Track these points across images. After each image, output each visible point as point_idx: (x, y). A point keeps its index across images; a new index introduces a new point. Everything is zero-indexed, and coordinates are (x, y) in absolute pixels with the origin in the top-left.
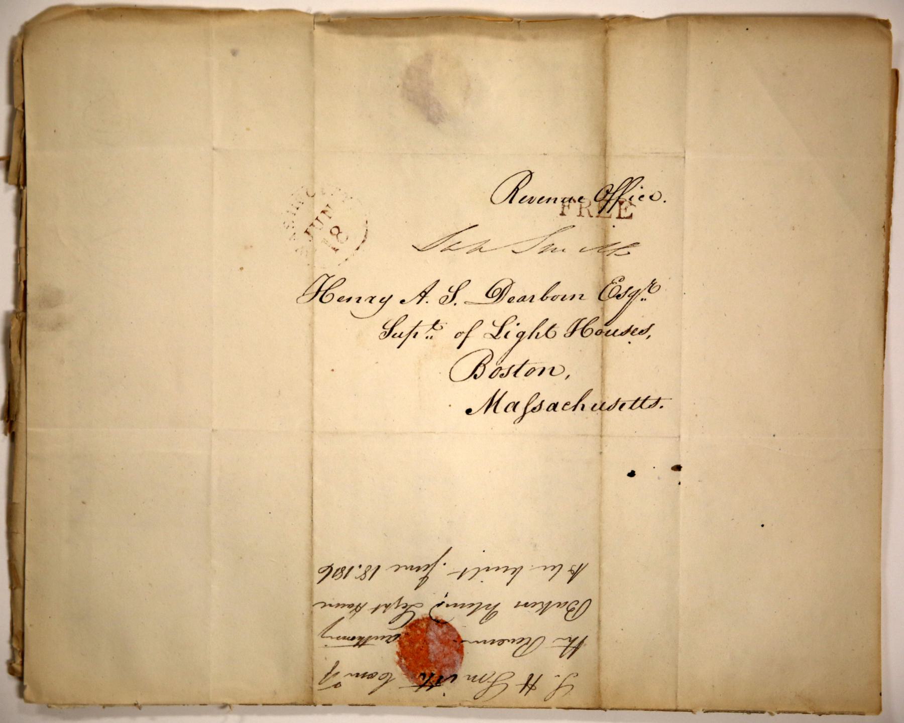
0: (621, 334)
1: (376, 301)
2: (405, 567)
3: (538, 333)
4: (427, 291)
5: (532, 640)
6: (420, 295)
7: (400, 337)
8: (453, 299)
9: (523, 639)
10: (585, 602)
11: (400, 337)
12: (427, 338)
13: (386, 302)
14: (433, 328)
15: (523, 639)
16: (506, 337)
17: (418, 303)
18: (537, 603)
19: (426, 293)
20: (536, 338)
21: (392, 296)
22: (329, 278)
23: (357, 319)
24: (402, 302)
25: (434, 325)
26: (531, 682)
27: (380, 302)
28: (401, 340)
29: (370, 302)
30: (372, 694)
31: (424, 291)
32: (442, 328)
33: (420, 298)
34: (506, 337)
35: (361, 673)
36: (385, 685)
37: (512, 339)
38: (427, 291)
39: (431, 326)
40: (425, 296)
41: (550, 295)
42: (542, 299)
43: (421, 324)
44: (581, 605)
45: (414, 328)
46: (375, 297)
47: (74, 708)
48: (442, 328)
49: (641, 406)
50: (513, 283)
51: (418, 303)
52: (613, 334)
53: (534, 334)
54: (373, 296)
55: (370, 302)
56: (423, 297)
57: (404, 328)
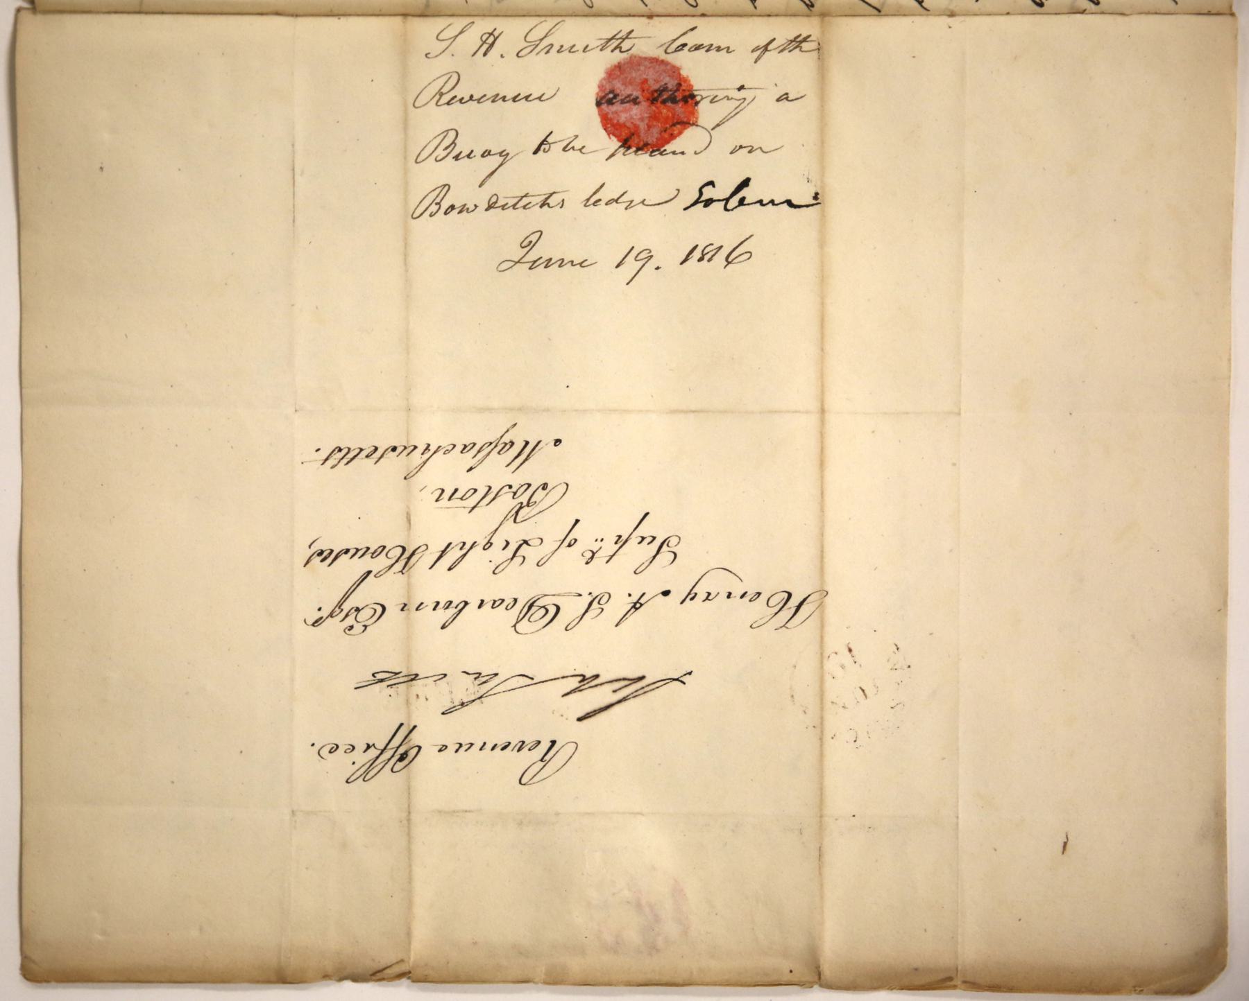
0: (347, 551)
1: (703, 596)
2: (764, 203)
3: (461, 549)
4: (633, 610)
5: (435, 102)
6: (641, 605)
7: (643, 538)
8: (594, 599)
9: (448, 103)
10: (423, 160)
11: (643, 538)
12: (602, 540)
13: (689, 594)
14: (594, 554)
15: (448, 103)
16: (508, 543)
17: (644, 594)
18: (671, 154)
19: (634, 607)
20: (464, 544)
21: (682, 603)
22: (784, 626)
23: (718, 567)
24: (666, 593)
25: (592, 558)
26: (485, 47)
27: (696, 594)
28: (640, 531)
29: (709, 594)
30: (692, 27)
31: (637, 609)
32: (583, 555)
33: (642, 601)
34: (508, 543)
35: (713, 53)
36: (675, 37)
37: (498, 541)
38: (633, 610)
39: (596, 555)
40: (635, 604)
41: (452, 611)
42: (466, 603)
43: (608, 558)
44: (433, 155)
45: (617, 554)
46: (704, 601)
47: (331, 11)
48: (583, 555)
49: (405, 448)
50: (515, 626)
51: (644, 594)
52: (358, 550)
53: (467, 549)
54: (707, 601)
55: (709, 594)
56: (638, 602)
57: (636, 553)
